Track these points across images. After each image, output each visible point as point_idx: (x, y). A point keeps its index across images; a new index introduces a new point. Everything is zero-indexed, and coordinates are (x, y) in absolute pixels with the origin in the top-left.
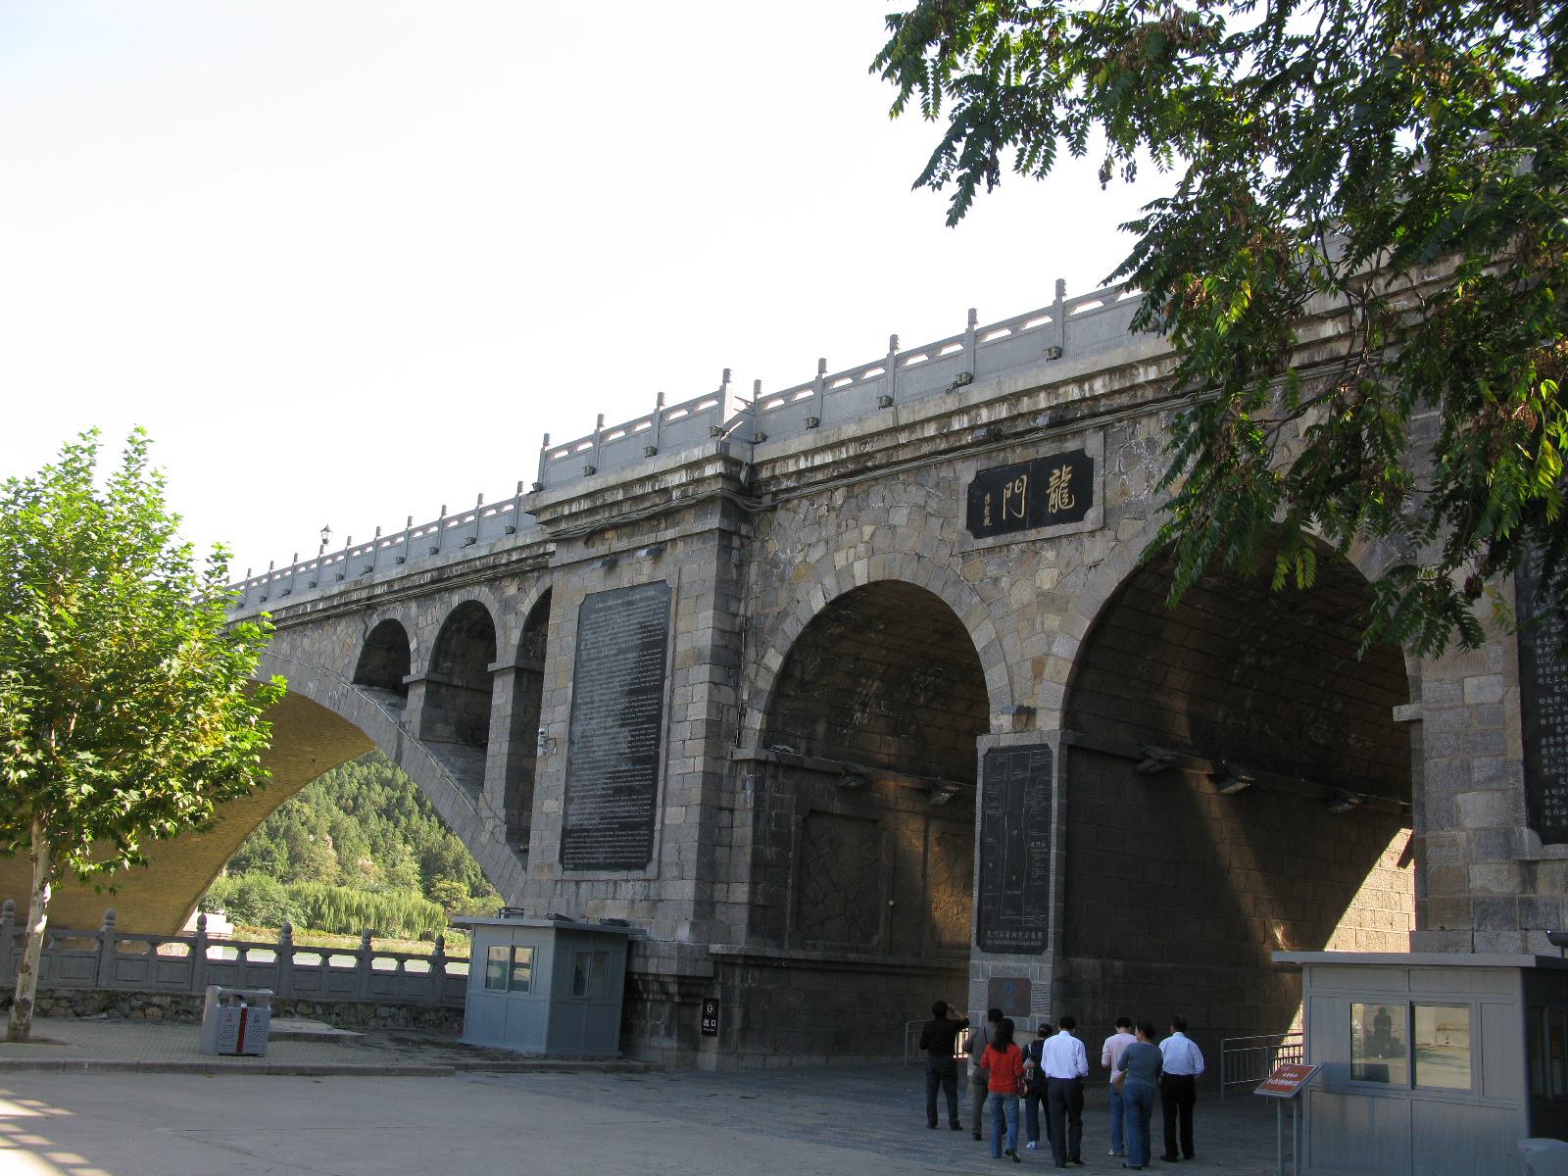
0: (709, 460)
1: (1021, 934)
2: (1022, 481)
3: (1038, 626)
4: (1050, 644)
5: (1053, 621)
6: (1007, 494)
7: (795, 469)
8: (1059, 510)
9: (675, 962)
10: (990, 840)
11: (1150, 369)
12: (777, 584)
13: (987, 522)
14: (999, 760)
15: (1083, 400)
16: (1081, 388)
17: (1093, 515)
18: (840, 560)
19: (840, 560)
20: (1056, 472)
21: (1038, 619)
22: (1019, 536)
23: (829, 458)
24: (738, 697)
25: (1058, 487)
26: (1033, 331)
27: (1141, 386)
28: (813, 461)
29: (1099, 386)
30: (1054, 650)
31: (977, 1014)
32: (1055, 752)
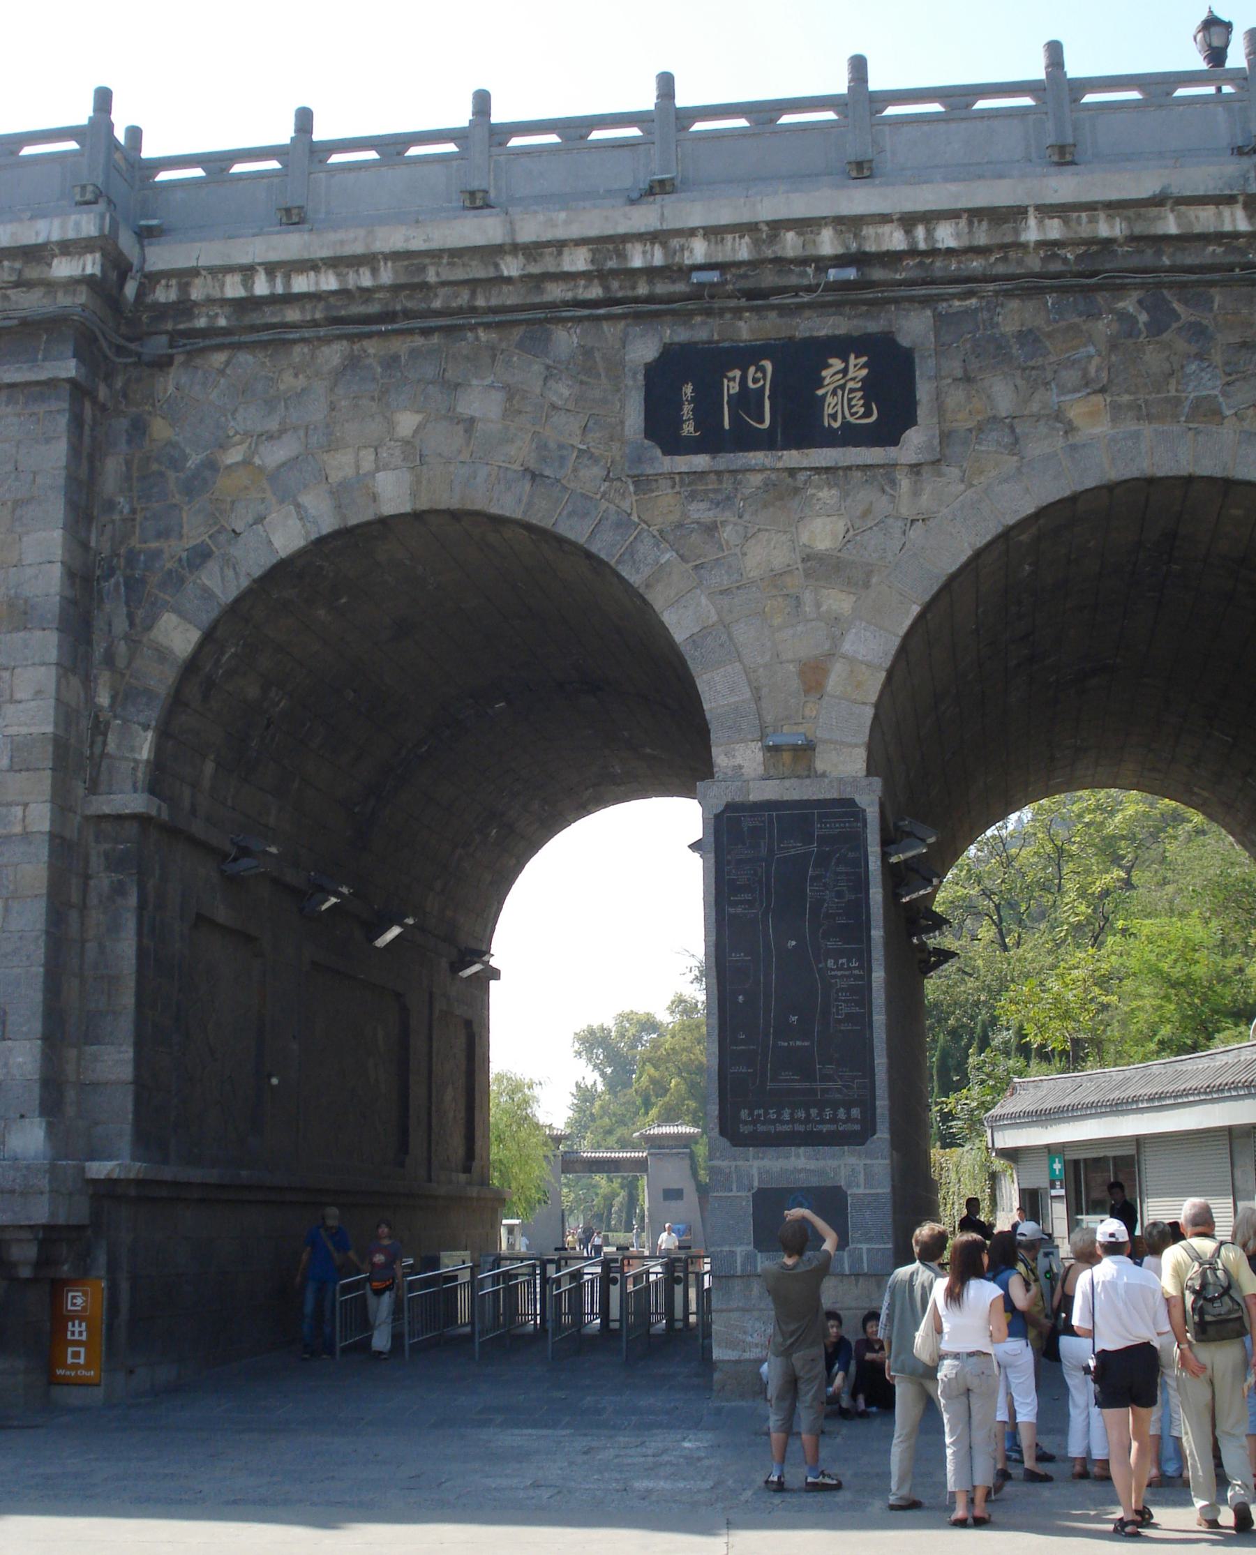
0: (67, 248)
1: (814, 1112)
2: (762, 369)
3: (808, 608)
4: (836, 641)
5: (838, 601)
6: (731, 387)
7: (241, 293)
8: (846, 424)
9: (45, 1198)
10: (735, 957)
11: (361, 270)
12: (177, 499)
13: (688, 429)
14: (747, 824)
15: (913, 252)
16: (909, 232)
17: (915, 442)
18: (341, 465)
19: (341, 465)
20: (837, 364)
21: (808, 597)
22: (757, 458)
23: (329, 282)
24: (90, 698)
25: (843, 387)
26: (241, 177)
27: (634, 273)
28: (287, 283)
29: (946, 236)
30: (847, 647)
31: (733, 1253)
32: (873, 816)
